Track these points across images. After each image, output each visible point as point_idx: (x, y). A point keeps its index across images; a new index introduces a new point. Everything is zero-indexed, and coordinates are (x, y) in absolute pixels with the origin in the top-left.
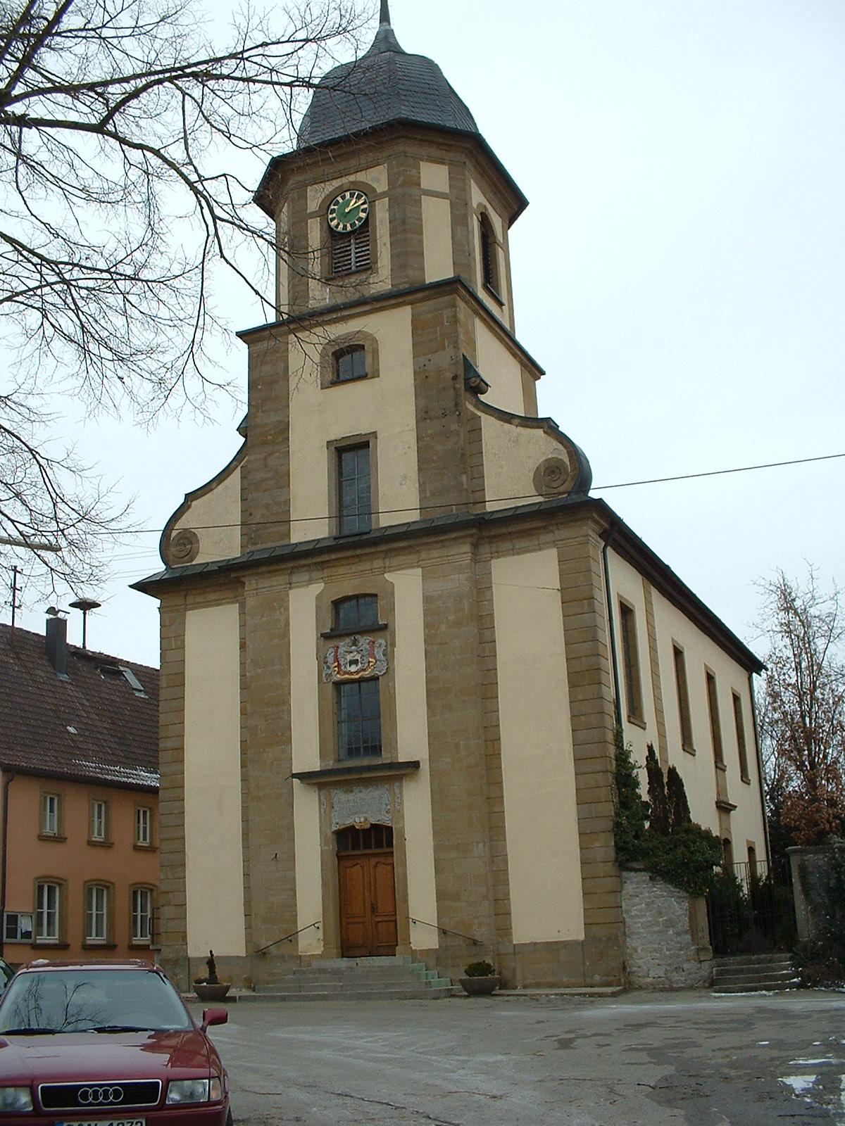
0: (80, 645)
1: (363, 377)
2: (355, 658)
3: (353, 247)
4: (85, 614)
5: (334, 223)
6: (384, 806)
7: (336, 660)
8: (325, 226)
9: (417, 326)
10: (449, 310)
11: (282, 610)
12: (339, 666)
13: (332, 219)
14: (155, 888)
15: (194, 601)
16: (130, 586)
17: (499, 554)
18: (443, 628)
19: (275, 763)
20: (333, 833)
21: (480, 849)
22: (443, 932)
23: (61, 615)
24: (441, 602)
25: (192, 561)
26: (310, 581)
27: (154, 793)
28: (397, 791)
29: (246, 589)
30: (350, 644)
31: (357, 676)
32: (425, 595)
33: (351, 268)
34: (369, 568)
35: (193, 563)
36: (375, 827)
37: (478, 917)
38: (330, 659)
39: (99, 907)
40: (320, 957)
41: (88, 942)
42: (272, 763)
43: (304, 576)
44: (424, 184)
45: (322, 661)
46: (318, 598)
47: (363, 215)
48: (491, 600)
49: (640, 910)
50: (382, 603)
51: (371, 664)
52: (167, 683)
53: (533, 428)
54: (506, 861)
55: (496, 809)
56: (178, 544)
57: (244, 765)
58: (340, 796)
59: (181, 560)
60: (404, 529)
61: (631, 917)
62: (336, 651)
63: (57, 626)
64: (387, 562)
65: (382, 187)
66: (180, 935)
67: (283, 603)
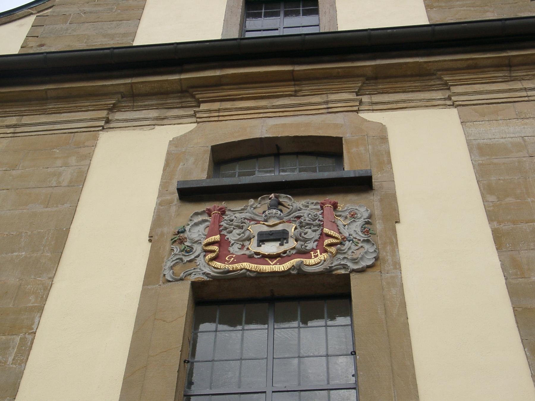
2: (280, 228)
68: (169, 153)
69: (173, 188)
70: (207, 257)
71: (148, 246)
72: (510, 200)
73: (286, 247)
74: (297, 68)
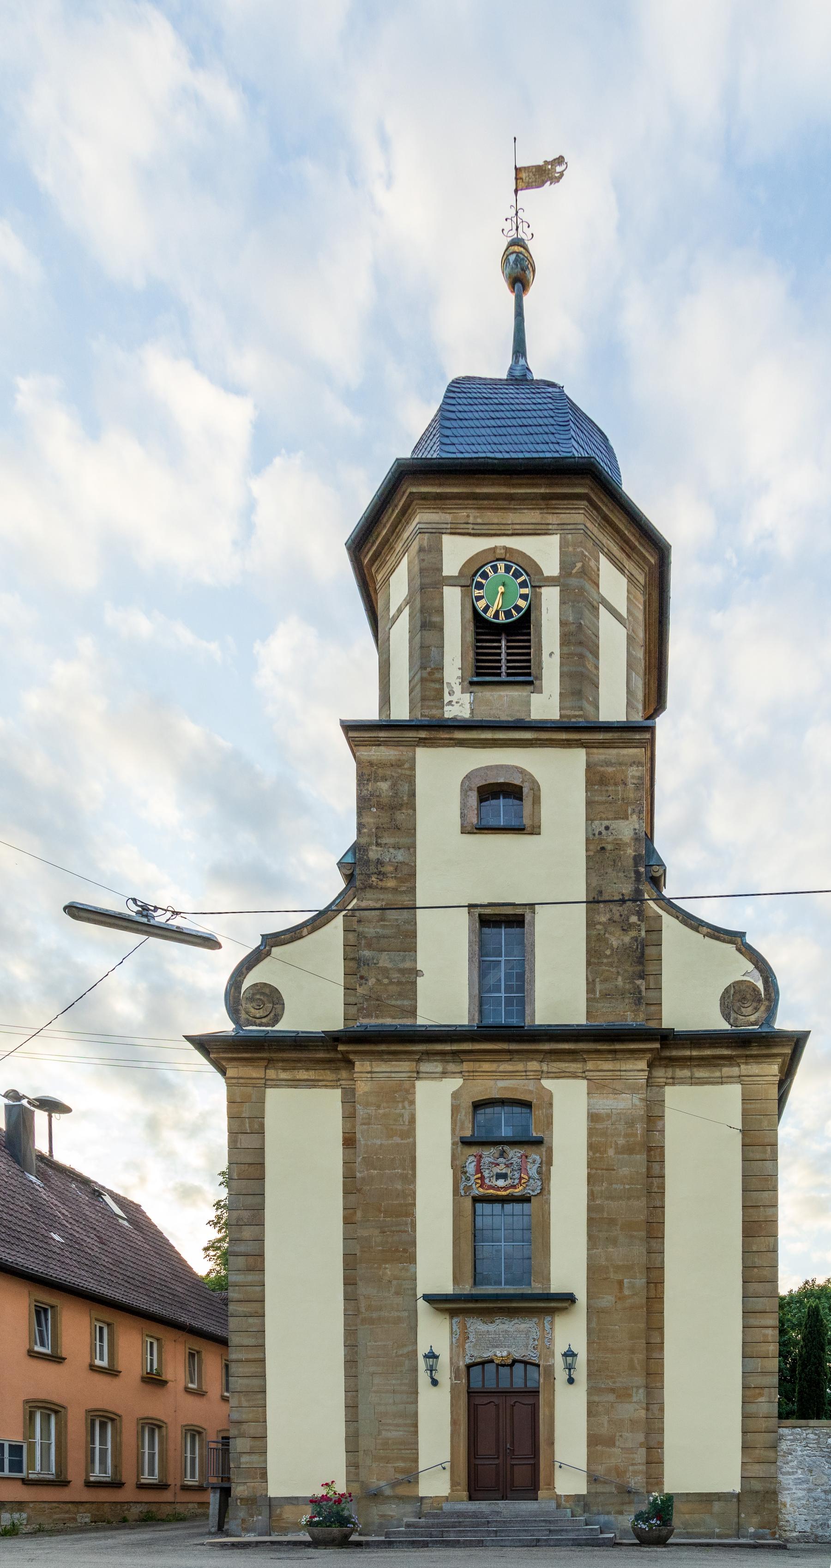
1: (519, 830)
2: (504, 1171)
3: (503, 643)
5: (481, 605)
6: (531, 1342)
7: (479, 1170)
11: (406, 1103)
12: (482, 1178)
13: (479, 598)
14: (164, 1425)
15: (277, 1075)
16: (188, 1038)
18: (611, 1152)
19: (394, 1282)
21: (640, 1395)
22: (593, 1479)
24: (609, 1122)
25: (273, 1026)
26: (444, 1074)
28: (547, 1326)
29: (356, 1070)
30: (497, 1155)
31: (504, 1193)
32: (591, 1111)
34: (524, 1069)
35: (275, 1028)
37: (633, 1465)
38: (471, 1168)
39: (103, 1442)
40: (447, 1499)
41: (92, 1479)
42: (390, 1282)
43: (435, 1067)
45: (459, 1171)
46: (455, 1095)
47: (522, 604)
48: (662, 1131)
49: (792, 1468)
50: (537, 1113)
51: (523, 1181)
54: (662, 1410)
55: (655, 1355)
57: (349, 1282)
58: (476, 1326)
59: (258, 1021)
60: (424, 1029)
62: (479, 1162)
64: (271, 1073)
65: (551, 567)
66: (258, 1471)
67: (408, 1096)
68: (452, 1105)
69: (458, 1139)
70: (513, 248)
71: (451, 1171)
72: (598, 1155)
73: (507, 1183)
74: (462, 1448)
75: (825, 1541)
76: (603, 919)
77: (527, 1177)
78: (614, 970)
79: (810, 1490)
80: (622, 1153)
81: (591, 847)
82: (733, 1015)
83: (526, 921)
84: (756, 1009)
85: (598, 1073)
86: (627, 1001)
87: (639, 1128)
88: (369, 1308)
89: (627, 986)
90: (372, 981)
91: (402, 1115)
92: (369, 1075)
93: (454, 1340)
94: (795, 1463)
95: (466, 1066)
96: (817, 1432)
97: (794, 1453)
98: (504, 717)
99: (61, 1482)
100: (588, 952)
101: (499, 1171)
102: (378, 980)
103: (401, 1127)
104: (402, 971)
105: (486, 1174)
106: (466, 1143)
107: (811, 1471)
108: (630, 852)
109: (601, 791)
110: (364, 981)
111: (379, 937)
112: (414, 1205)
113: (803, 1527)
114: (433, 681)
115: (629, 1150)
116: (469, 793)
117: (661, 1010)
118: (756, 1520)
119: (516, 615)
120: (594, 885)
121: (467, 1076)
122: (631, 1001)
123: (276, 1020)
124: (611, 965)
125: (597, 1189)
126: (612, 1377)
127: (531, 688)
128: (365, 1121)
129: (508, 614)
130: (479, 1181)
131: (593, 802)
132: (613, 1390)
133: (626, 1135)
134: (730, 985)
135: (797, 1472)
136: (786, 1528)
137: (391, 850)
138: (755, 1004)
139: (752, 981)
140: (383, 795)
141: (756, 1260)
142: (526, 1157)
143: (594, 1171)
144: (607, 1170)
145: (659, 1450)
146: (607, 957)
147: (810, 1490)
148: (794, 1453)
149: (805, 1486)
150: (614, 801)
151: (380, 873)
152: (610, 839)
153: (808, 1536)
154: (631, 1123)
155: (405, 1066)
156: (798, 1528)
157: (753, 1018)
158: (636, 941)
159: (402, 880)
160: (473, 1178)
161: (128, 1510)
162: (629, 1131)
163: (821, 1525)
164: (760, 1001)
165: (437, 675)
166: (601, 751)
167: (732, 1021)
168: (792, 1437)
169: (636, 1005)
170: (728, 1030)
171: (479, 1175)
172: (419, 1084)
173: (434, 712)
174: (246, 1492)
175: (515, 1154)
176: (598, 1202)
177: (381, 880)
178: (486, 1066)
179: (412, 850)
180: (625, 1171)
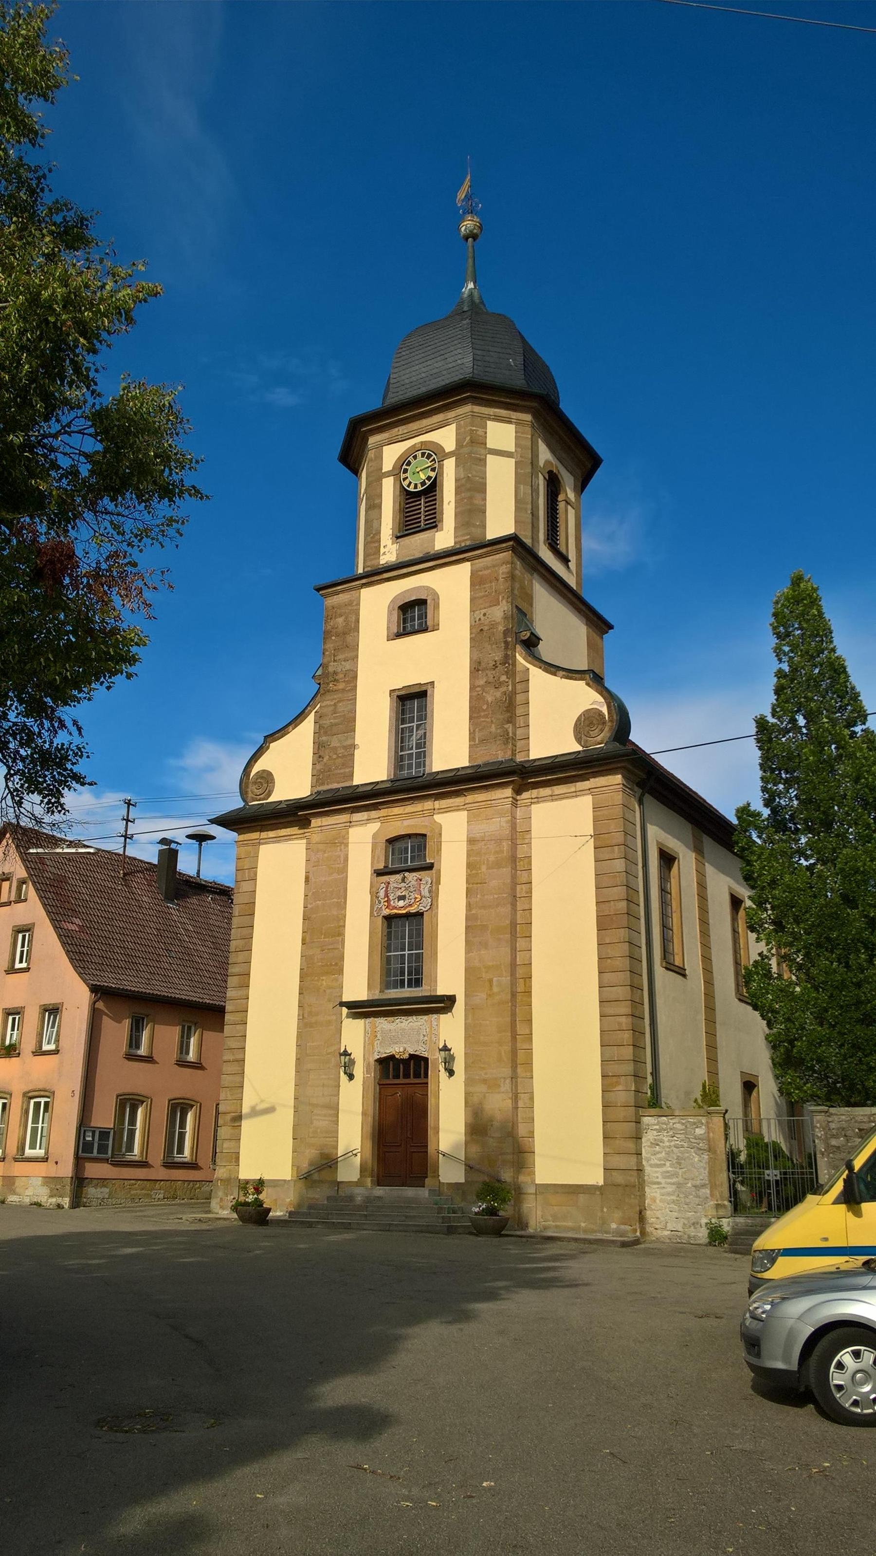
0: (193, 872)
2: (403, 894)
4: (200, 845)
7: (387, 895)
8: (398, 486)
9: (476, 581)
10: (504, 566)
12: (388, 901)
13: (405, 479)
17: (538, 800)
18: (484, 868)
20: (376, 1061)
21: (507, 1086)
23: (173, 846)
27: (220, 1012)
33: (420, 526)
36: (412, 1056)
37: (502, 1154)
38: (382, 894)
44: (490, 444)
45: (374, 895)
46: (375, 836)
49: (660, 1160)
52: (239, 913)
53: (576, 679)
56: (255, 783)
58: (382, 1023)
61: (651, 1166)
62: (387, 888)
63: (170, 855)
64: (264, 835)
65: (450, 445)
66: (234, 1156)
71: (370, 896)
75: (699, 1242)
76: (482, 682)
77: (420, 897)
78: (489, 720)
79: (679, 1185)
80: (493, 868)
81: (474, 631)
82: (584, 737)
83: (428, 695)
84: (602, 731)
85: (475, 805)
86: (498, 742)
87: (506, 845)
88: (310, 1013)
89: (499, 731)
90: (326, 758)
91: (339, 857)
92: (319, 829)
93: (367, 1038)
94: (663, 1154)
95: (383, 812)
96: (684, 1121)
97: (661, 1144)
98: (418, 555)
99: (143, 1164)
100: (471, 708)
101: (401, 894)
102: (330, 757)
103: (338, 866)
104: (345, 748)
105: (391, 898)
106: (379, 873)
107: (680, 1164)
108: (501, 628)
109: (480, 589)
110: (321, 759)
111: (332, 725)
112: (344, 926)
113: (674, 1225)
114: (374, 542)
115: (498, 865)
116: (393, 612)
117: (529, 744)
118: (617, 1215)
119: (428, 483)
120: (475, 658)
121: (383, 820)
122: (501, 742)
123: (269, 795)
124: (486, 716)
125: (473, 900)
126: (483, 1068)
127: (436, 529)
128: (316, 864)
129: (423, 484)
130: (386, 904)
131: (475, 598)
132: (485, 1081)
133: (496, 852)
134: (581, 715)
135: (665, 1165)
136: (657, 1226)
137: (343, 663)
138: (600, 727)
139: (598, 707)
140: (340, 627)
141: (609, 951)
142: (421, 880)
143: (471, 886)
144: (480, 883)
145: (530, 1139)
146: (484, 711)
147: (679, 1185)
148: (661, 1144)
149: (674, 1180)
150: (490, 594)
151: (335, 680)
152: (487, 622)
153: (681, 1236)
154: (499, 841)
155: (344, 818)
156: (670, 1226)
157: (599, 738)
158: (505, 694)
159: (348, 682)
160: (382, 901)
161: (200, 1188)
162: (498, 849)
163: (693, 1224)
164: (604, 723)
165: (377, 537)
166: (480, 560)
167: (582, 743)
168: (657, 1127)
169: (505, 744)
170: (579, 752)
171: (386, 899)
172: (351, 830)
173: (374, 562)
174: (225, 1174)
175: (412, 877)
176: (473, 912)
177: (335, 685)
178: (396, 810)
179: (355, 660)
180: (494, 883)
